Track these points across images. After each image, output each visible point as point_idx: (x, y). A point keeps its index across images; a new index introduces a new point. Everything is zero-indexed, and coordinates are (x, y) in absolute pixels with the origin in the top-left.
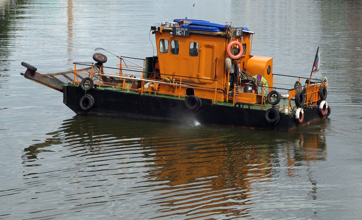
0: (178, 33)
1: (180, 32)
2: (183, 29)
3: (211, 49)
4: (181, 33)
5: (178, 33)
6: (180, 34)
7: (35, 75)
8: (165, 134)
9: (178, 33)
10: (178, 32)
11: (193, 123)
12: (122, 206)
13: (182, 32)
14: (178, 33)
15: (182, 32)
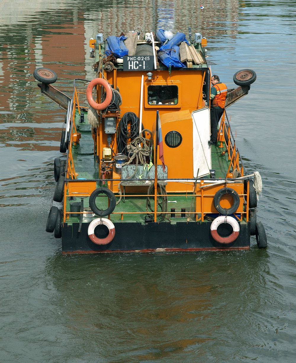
0: (132, 66)
1: (136, 63)
2: (141, 59)
3: (200, 198)
4: (136, 65)
5: (131, 67)
6: (136, 67)
7: (49, 89)
8: (149, 150)
9: (131, 67)
10: (131, 64)
11: (10, 132)
12: (124, 340)
13: (139, 64)
14: (132, 66)
15: (139, 64)
